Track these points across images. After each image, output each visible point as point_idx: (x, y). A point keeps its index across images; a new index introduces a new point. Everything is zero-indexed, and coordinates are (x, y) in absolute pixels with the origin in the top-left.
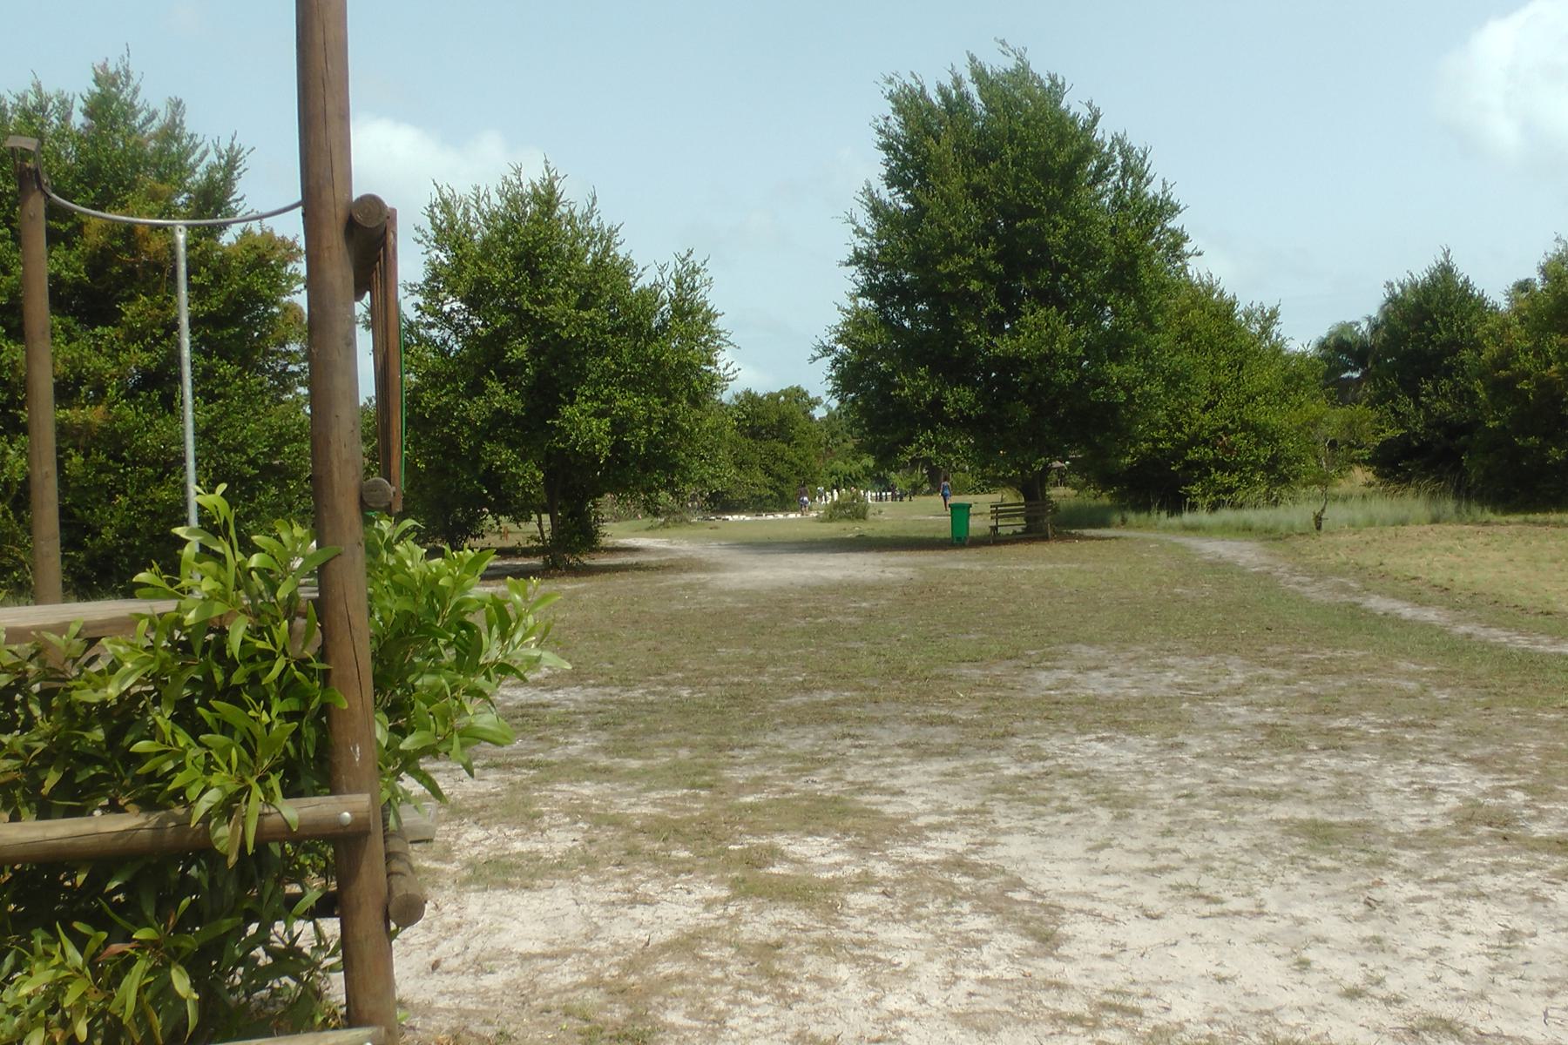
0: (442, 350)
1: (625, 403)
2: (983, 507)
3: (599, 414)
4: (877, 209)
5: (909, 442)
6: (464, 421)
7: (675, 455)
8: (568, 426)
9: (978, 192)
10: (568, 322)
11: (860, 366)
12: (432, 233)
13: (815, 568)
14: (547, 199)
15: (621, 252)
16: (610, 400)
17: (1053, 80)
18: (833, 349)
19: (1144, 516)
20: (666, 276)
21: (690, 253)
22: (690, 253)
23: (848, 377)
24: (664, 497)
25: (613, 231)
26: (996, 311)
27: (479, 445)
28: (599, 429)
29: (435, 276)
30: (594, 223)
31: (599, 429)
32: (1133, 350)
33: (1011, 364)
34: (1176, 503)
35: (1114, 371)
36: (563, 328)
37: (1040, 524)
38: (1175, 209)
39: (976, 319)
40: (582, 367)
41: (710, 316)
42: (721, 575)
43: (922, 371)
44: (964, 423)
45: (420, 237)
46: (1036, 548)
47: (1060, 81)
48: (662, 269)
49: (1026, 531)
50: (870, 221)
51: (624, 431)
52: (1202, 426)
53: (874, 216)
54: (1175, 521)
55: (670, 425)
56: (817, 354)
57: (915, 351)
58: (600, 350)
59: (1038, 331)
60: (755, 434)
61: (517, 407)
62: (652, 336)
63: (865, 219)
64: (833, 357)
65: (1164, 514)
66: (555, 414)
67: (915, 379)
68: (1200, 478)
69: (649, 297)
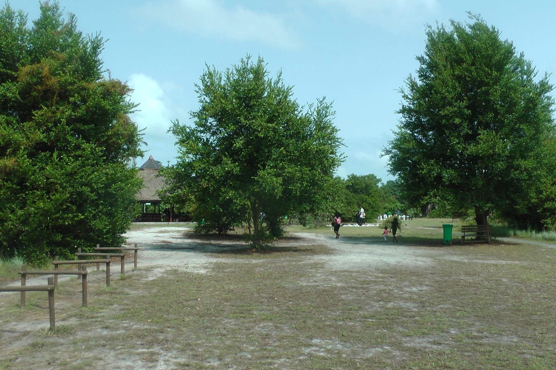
0: (206, 144)
1: (290, 170)
2: (457, 225)
3: (277, 175)
4: (413, 86)
5: (426, 195)
6: (212, 176)
7: (314, 197)
8: (261, 180)
9: (458, 78)
10: (262, 129)
11: (404, 159)
12: (202, 87)
13: (381, 255)
14: (258, 73)
15: (291, 98)
16: (283, 168)
17: (494, 28)
18: (390, 152)
19: (524, 232)
20: (312, 109)
21: (324, 98)
22: (324, 98)
23: (398, 165)
24: (309, 216)
25: (289, 89)
26: (467, 133)
27: (219, 189)
28: (277, 183)
29: (204, 108)
30: (280, 85)
31: (277, 183)
32: (532, 154)
33: (474, 159)
34: (540, 227)
35: (523, 163)
36: (259, 132)
37: (482, 236)
38: (550, 88)
39: (458, 137)
40: (270, 152)
41: (334, 130)
42: (333, 258)
43: (432, 162)
44: (452, 186)
45: (198, 90)
46: (484, 248)
47: (496, 30)
48: (311, 106)
49: (478, 239)
50: (410, 92)
51: (289, 184)
52: (551, 192)
53: (412, 90)
54: (540, 235)
55: (313, 183)
56: (383, 153)
57: (429, 153)
58: (280, 145)
59: (487, 141)
60: (355, 191)
61: (237, 170)
62: (304, 138)
63: (408, 91)
64: (390, 155)
65: (534, 232)
66: (255, 174)
67: (429, 165)
68: (550, 216)
69: (305, 122)
